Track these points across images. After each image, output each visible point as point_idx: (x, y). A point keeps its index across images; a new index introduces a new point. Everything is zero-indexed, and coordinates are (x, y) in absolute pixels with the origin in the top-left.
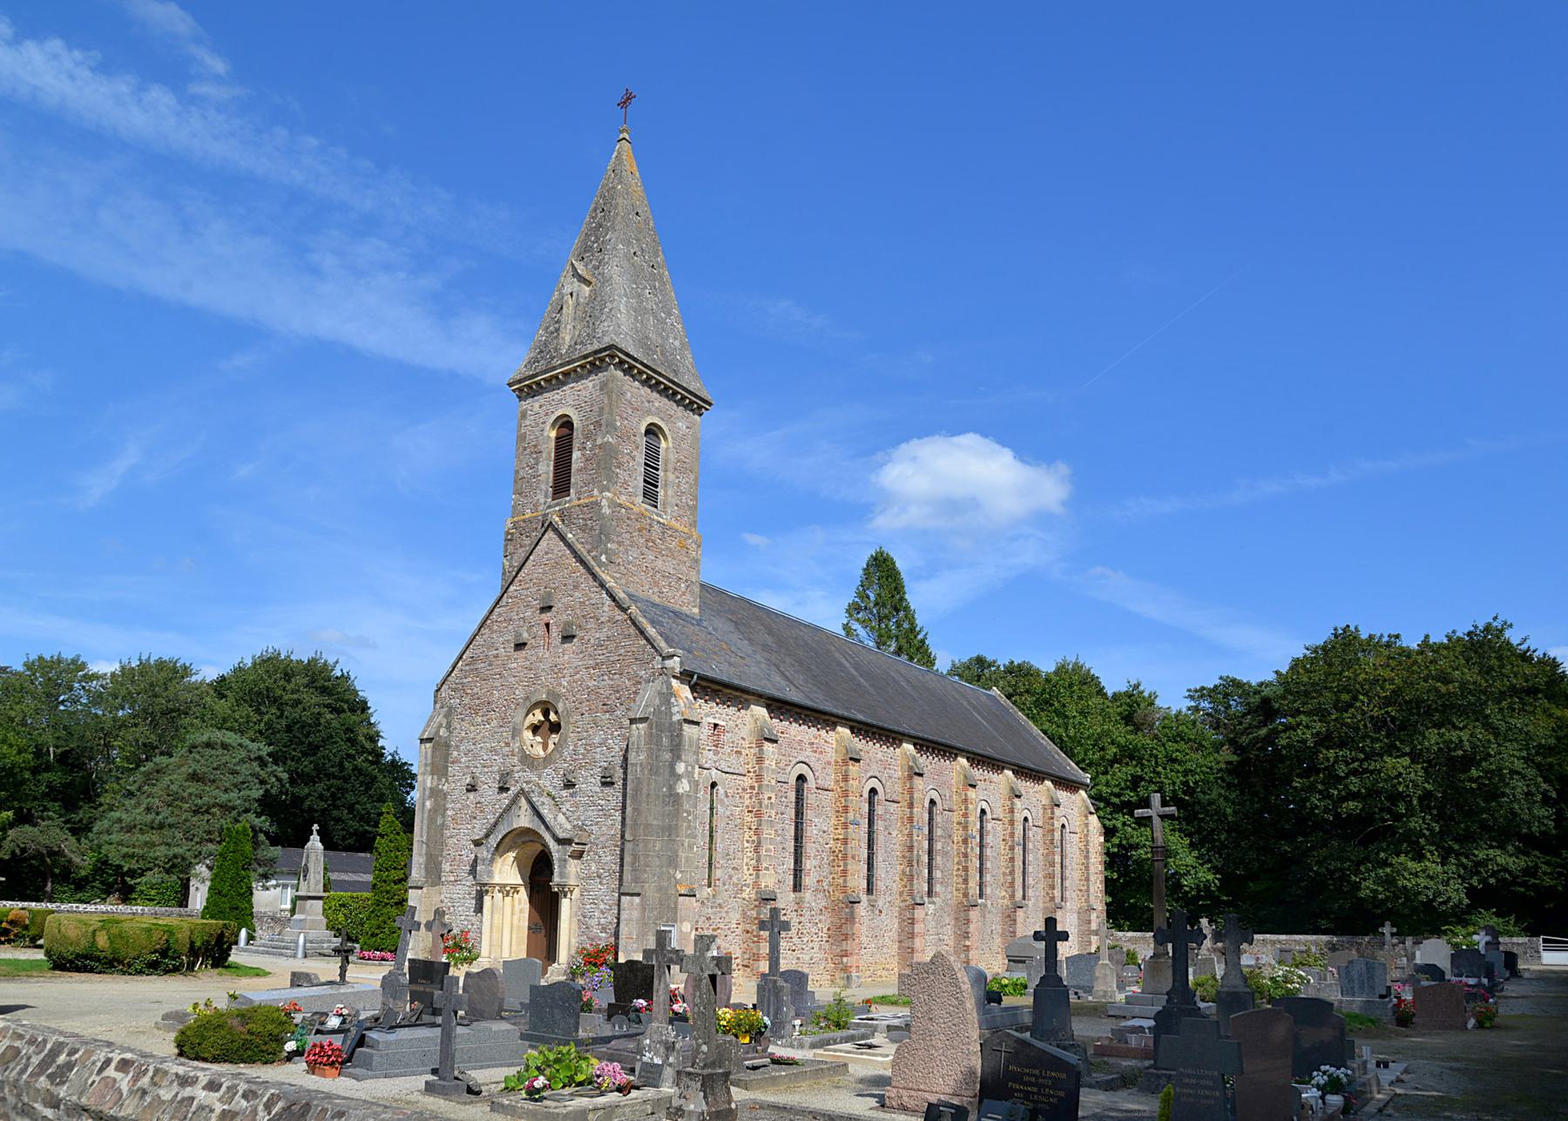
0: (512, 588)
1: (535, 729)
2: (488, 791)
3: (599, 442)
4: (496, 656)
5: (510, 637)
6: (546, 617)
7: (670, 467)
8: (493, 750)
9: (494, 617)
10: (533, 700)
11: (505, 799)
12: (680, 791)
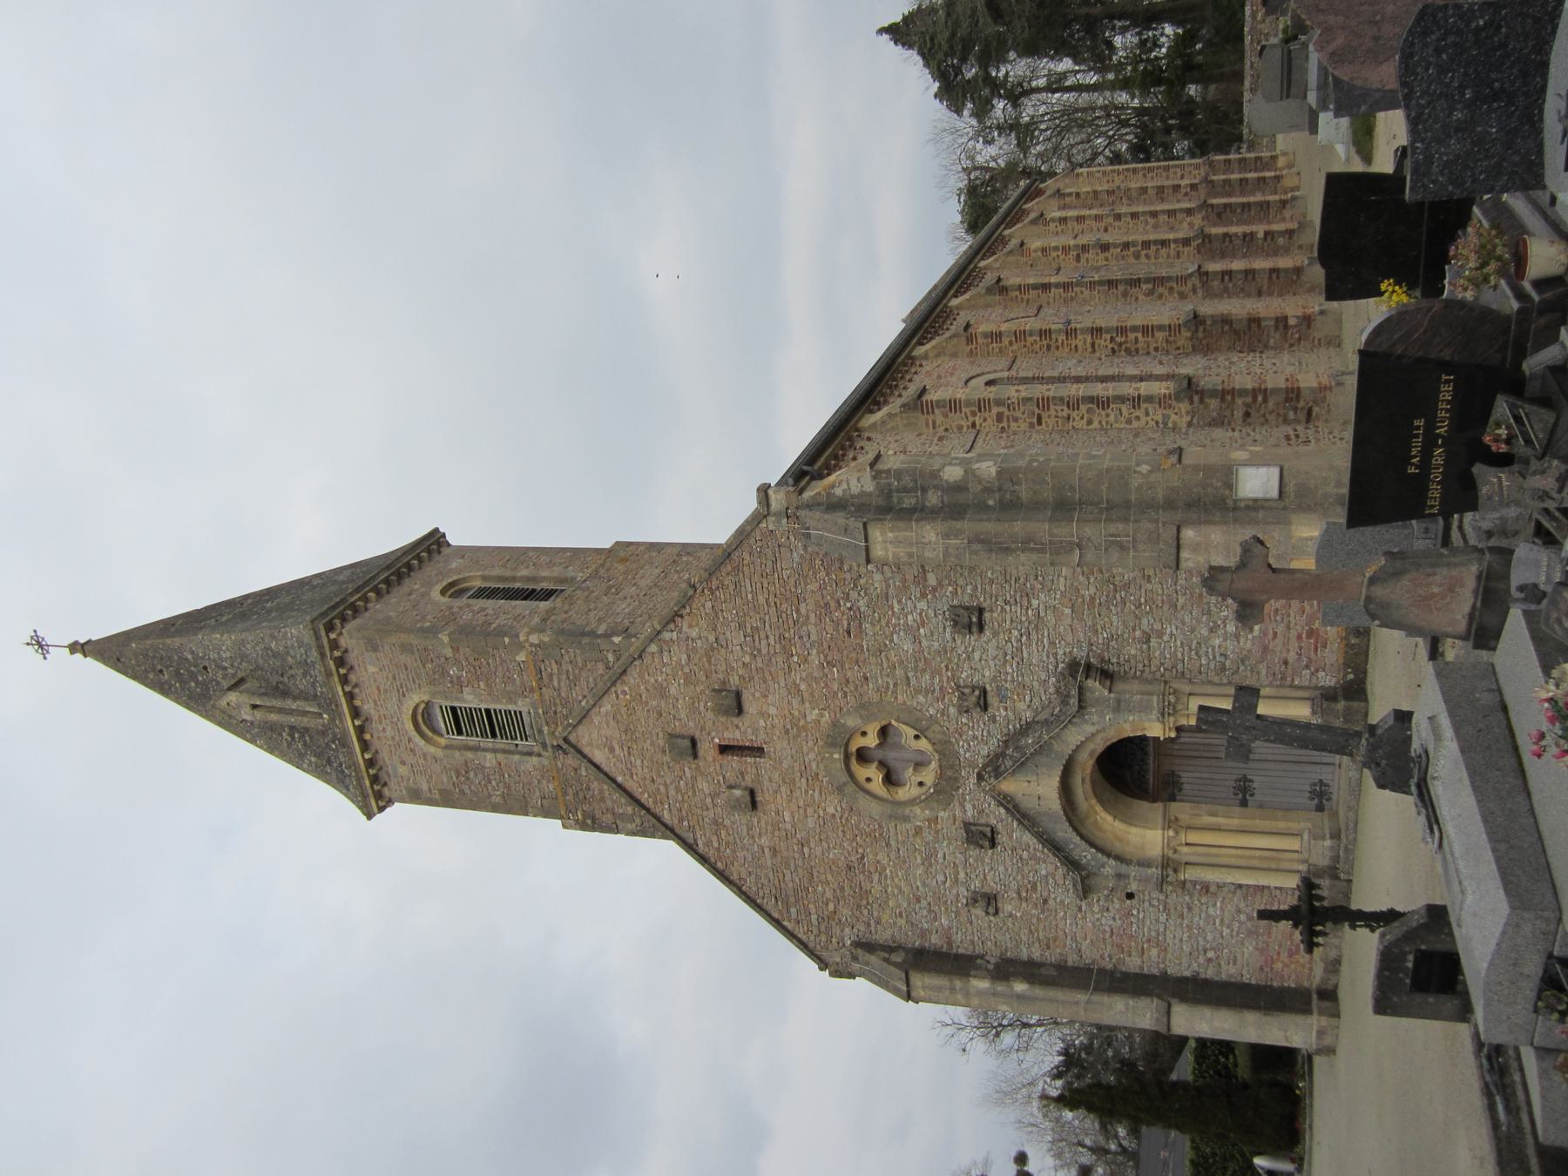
0: (666, 816)
1: (890, 780)
2: (993, 870)
3: (448, 652)
4: (774, 852)
5: (740, 819)
6: (707, 750)
7: (508, 573)
8: (928, 860)
9: (712, 854)
10: (844, 777)
11: (1014, 834)
12: (993, 471)
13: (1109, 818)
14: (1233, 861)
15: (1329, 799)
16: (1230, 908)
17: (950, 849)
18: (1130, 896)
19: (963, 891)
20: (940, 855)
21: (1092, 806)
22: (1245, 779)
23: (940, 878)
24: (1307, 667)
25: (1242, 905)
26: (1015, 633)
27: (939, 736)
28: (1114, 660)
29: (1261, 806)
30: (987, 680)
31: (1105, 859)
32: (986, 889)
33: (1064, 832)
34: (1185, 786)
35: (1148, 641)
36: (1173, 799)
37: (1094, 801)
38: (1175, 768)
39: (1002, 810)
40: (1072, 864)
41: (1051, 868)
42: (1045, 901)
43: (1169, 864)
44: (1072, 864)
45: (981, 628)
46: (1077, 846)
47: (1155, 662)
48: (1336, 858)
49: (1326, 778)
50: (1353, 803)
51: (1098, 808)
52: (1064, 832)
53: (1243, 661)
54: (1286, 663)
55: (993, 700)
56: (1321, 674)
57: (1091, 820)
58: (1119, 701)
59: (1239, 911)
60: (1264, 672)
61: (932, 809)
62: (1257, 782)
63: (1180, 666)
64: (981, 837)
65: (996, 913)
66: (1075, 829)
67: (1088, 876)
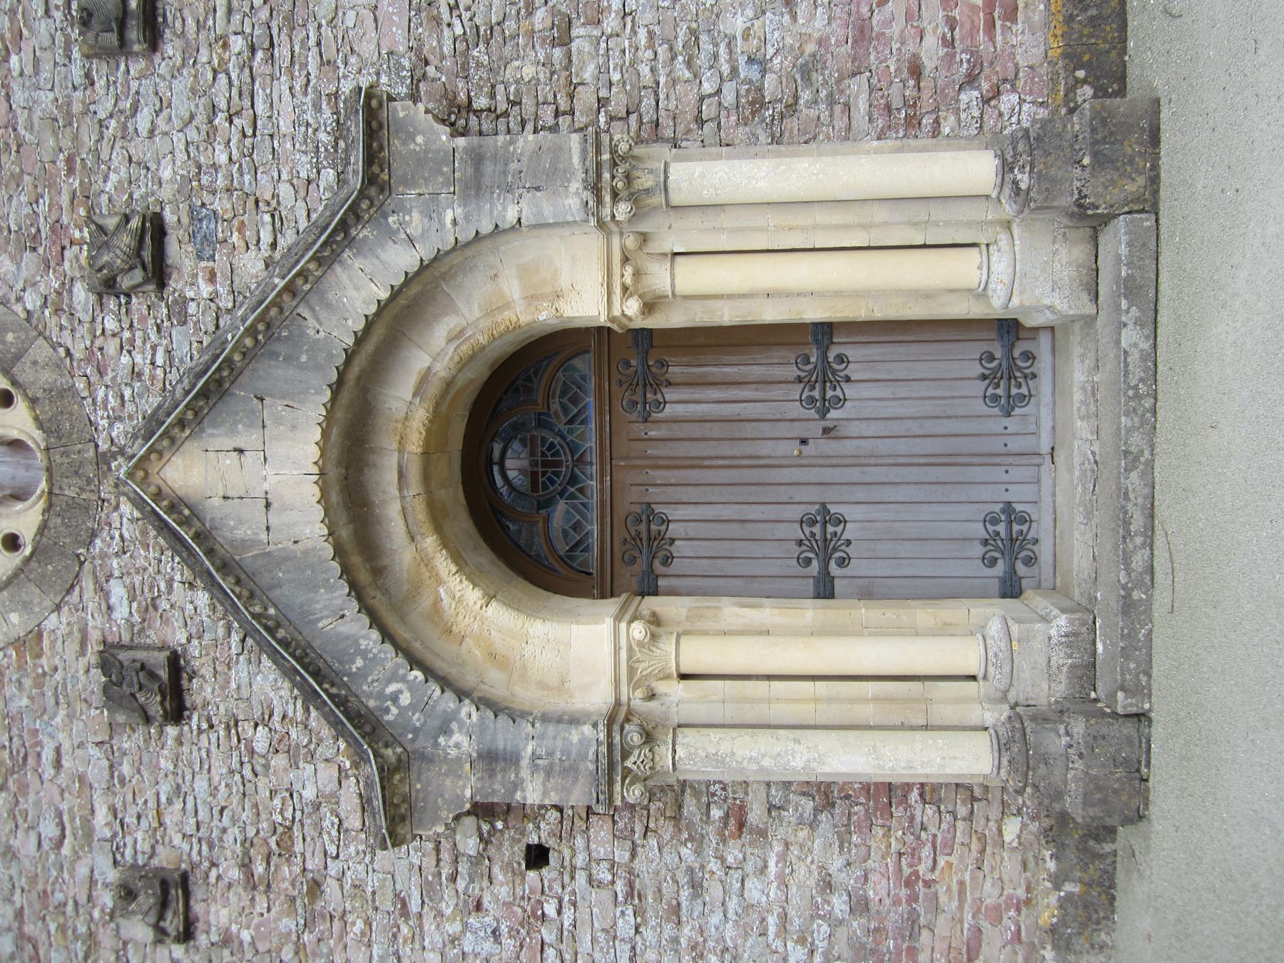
13: (473, 596)
14: (806, 712)
15: (1030, 561)
16: (805, 876)
17: (76, 733)
18: (537, 856)
19: (103, 863)
20: (48, 755)
21: (426, 561)
22: (825, 517)
23: (49, 829)
24: (971, 80)
25: (836, 863)
26: (238, 44)
27: (47, 377)
28: (481, 102)
29: (867, 593)
30: (166, 193)
31: (449, 702)
32: (164, 858)
33: (337, 619)
34: (680, 548)
35: (564, 40)
36: (649, 588)
37: (430, 541)
38: (655, 494)
39: (203, 598)
40: (360, 724)
41: (327, 774)
42: (315, 888)
43: (628, 732)
44: (360, 724)
45: (154, 40)
46: (372, 662)
47: (586, 98)
48: (1086, 672)
49: (1016, 494)
50: (1136, 440)
51: (444, 564)
52: (337, 619)
53: (806, 72)
54: (916, 71)
55: (179, 252)
56: (1008, 100)
57: (425, 602)
58: (477, 159)
59: (827, 885)
60: (862, 105)
61: (26, 607)
62: (858, 522)
63: (648, 102)
64: (155, 689)
65: (187, 935)
66: (376, 621)
67: (402, 765)
